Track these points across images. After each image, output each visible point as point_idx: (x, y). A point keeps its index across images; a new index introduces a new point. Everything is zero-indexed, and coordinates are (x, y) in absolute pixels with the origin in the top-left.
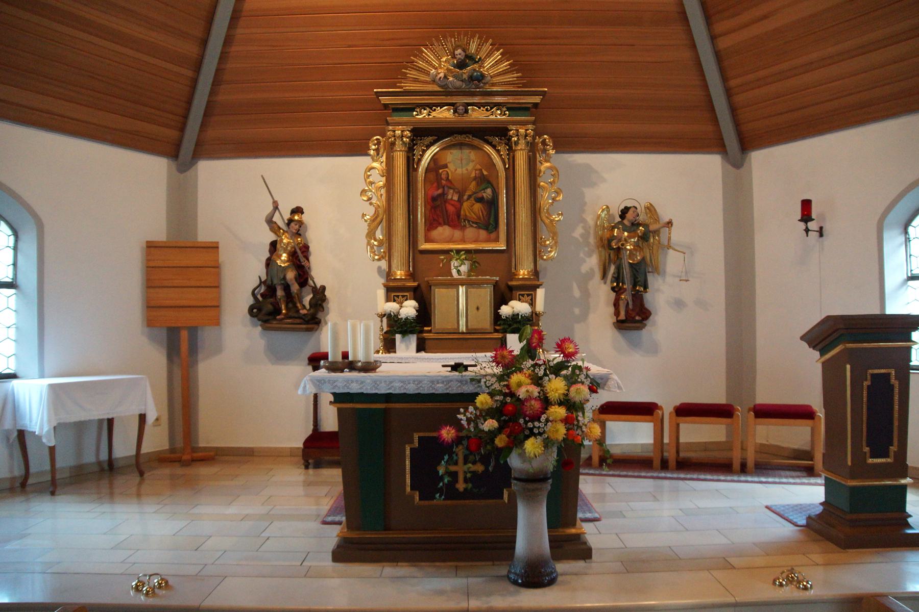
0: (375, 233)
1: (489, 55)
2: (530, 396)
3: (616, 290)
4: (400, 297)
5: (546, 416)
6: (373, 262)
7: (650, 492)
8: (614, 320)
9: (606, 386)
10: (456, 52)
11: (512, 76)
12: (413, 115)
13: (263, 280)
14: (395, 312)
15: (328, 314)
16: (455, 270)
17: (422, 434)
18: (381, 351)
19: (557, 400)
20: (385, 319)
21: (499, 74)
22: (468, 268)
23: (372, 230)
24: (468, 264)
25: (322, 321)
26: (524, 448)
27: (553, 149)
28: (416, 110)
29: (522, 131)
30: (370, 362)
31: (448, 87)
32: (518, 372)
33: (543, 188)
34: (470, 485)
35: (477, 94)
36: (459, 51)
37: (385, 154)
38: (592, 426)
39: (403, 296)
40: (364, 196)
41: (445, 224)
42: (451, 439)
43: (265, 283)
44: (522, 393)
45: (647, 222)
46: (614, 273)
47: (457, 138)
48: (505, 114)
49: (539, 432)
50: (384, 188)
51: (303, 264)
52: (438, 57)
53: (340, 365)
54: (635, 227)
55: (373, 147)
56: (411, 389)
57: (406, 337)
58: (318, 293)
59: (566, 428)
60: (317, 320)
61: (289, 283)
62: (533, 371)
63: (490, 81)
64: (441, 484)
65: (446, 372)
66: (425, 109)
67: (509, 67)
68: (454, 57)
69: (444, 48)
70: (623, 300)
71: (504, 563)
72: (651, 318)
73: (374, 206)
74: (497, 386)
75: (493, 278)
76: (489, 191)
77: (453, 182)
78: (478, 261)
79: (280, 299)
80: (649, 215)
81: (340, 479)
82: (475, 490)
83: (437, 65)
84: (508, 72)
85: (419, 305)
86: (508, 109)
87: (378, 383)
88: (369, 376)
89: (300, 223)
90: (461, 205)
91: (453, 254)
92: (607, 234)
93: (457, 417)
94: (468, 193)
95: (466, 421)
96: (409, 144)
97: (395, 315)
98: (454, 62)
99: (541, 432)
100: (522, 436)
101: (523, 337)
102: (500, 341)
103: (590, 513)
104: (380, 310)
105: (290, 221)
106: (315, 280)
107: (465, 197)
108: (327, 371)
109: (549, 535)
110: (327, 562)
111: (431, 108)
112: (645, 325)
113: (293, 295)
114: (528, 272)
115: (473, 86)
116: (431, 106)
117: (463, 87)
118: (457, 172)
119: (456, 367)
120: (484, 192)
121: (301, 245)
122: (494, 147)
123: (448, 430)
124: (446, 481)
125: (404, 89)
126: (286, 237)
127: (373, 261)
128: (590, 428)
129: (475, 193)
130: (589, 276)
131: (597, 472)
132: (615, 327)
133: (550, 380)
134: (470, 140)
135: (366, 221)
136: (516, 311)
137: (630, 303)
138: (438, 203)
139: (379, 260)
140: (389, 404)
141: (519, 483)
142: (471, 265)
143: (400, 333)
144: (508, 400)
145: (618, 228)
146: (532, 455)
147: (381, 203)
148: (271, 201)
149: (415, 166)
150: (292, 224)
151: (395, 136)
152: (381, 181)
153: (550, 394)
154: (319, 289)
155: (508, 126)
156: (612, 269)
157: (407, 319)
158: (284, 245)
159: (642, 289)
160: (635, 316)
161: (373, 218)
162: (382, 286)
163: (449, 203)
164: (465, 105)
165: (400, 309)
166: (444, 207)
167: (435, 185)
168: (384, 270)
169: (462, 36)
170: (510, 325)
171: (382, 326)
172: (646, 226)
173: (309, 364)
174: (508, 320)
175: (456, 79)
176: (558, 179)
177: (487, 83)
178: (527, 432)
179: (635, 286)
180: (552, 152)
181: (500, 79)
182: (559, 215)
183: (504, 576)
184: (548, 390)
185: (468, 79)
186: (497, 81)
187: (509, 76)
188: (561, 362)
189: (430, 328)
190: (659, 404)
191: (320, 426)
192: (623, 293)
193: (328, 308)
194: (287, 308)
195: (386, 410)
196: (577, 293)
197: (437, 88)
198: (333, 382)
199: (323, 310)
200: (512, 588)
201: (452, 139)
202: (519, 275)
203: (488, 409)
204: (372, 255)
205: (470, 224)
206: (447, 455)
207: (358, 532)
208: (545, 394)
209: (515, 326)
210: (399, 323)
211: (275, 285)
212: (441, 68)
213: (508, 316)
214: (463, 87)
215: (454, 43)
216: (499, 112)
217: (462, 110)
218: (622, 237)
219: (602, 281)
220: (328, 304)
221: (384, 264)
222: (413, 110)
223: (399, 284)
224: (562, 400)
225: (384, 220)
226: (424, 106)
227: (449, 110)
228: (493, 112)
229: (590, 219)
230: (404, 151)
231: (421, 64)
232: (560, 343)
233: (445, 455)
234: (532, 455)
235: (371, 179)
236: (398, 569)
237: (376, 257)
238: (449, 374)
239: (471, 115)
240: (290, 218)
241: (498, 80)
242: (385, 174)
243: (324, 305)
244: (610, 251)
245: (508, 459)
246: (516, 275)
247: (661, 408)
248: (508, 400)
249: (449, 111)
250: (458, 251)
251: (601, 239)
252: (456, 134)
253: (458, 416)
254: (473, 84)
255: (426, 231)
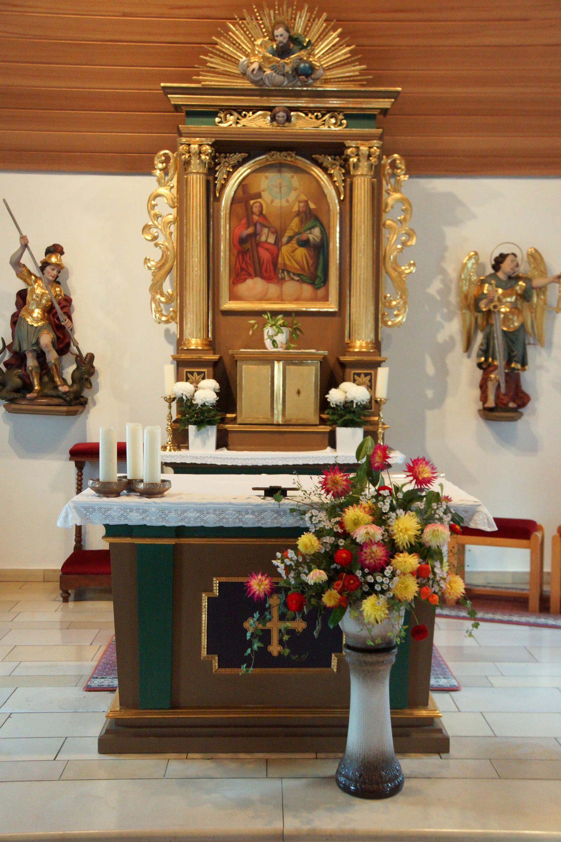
0: (162, 285)
1: (323, 36)
2: (371, 540)
3: (484, 366)
4: (195, 374)
5: (392, 568)
6: (159, 325)
7: (525, 647)
8: (480, 405)
9: (472, 521)
10: (277, 32)
11: (353, 68)
12: (215, 121)
13: (7, 344)
14: (188, 395)
15: (97, 391)
16: (269, 340)
17: (224, 579)
18: (168, 448)
19: (407, 544)
20: (174, 404)
21: (335, 65)
22: (286, 337)
23: (158, 282)
24: (287, 332)
25: (90, 401)
26: (361, 610)
27: (405, 174)
28: (219, 115)
29: (364, 149)
30: (156, 484)
31: (264, 83)
32: (355, 505)
33: (390, 228)
34: (287, 651)
35: (303, 94)
36: (280, 31)
37: (176, 176)
38: (454, 579)
39: (199, 373)
40: (147, 234)
41: (256, 276)
42: (263, 594)
43: (10, 347)
44: (360, 535)
45: (530, 275)
46: (482, 344)
47: (275, 157)
48: (341, 124)
49: (382, 589)
50: (174, 224)
51: (63, 324)
52: (250, 38)
53: (115, 487)
54: (514, 282)
55: (160, 166)
56: (211, 521)
57: (203, 430)
58: (85, 364)
59: (418, 583)
60: (82, 400)
61: (43, 349)
62: (375, 504)
63: (322, 75)
64: (249, 651)
65: (257, 499)
66: (231, 115)
67: (349, 55)
68: (273, 39)
69: (260, 25)
70: (492, 380)
71: (331, 755)
72: (530, 404)
73: (161, 248)
74: (327, 525)
75: (320, 352)
76: (317, 231)
77: (268, 217)
78: (301, 329)
79: (31, 372)
80: (533, 266)
81: (111, 618)
82: (294, 658)
83: (249, 51)
84: (349, 63)
85: (220, 386)
86: (346, 117)
87: (166, 512)
88: (155, 503)
89: (59, 267)
90: (279, 250)
91: (266, 317)
92: (474, 291)
93: (272, 563)
94: (288, 233)
95: (284, 570)
96: (209, 163)
97: (188, 400)
98: (272, 46)
99: (385, 589)
100: (358, 593)
101: (362, 453)
102: (327, 436)
103: (445, 678)
104: (168, 393)
105: (45, 265)
106: (80, 346)
107: (285, 240)
108: (97, 495)
109: (392, 718)
110: (93, 754)
111: (240, 113)
112: (521, 415)
113: (50, 365)
114: (367, 343)
115: (299, 83)
116: (239, 110)
117: (285, 83)
118: (274, 204)
119: (271, 492)
120: (311, 233)
121: (61, 297)
122: (325, 170)
123: (260, 580)
124: (255, 647)
125: (203, 85)
126: (39, 285)
127: (159, 323)
128: (450, 583)
129: (297, 234)
130: (449, 345)
131: (453, 613)
132: (481, 416)
133: (397, 518)
134: (292, 159)
135: (149, 268)
136: (350, 397)
137: (503, 385)
138: (248, 246)
139: (167, 322)
140: (181, 539)
141: (353, 653)
142: (291, 334)
143: (195, 423)
144: (341, 542)
145: (490, 284)
146: (372, 620)
147: (171, 244)
148: (19, 235)
149: (218, 195)
150: (48, 269)
151: (189, 152)
152: (171, 214)
153: (397, 536)
154: (86, 358)
155: (345, 142)
156: (480, 338)
157: (204, 405)
158: (38, 297)
159: (519, 366)
160: (508, 403)
161: (159, 265)
162: (171, 359)
163: (262, 247)
164: (286, 109)
165: (195, 391)
166: (255, 254)
167: (244, 221)
168: (174, 333)
169: (285, 7)
170: (341, 416)
171: (170, 413)
172: (527, 280)
173: (71, 459)
174: (339, 409)
175: (275, 72)
176: (411, 214)
177: (318, 79)
178: (366, 588)
179: (509, 362)
180: (404, 178)
181: (337, 74)
182: (410, 265)
183: (330, 778)
184: (395, 531)
185: (292, 74)
186: (332, 77)
187: (348, 69)
188: (412, 490)
189: (234, 415)
190: (539, 522)
191: (85, 542)
192: (492, 372)
193: (98, 384)
194: (41, 383)
195: (175, 546)
196: (430, 369)
197: (248, 85)
198: (105, 510)
199: (91, 388)
200: (343, 797)
201: (269, 157)
202: (354, 347)
203: (314, 555)
204: (157, 315)
205: (290, 276)
206: (257, 613)
207: (134, 711)
208: (390, 536)
209: (348, 417)
210: (193, 410)
211: (25, 351)
212: (255, 55)
213: (338, 404)
214: (285, 83)
215: (274, 18)
216: (333, 121)
217: (283, 117)
218: (494, 297)
219: (466, 354)
220: (97, 378)
221: (174, 327)
222: (215, 114)
223: (195, 356)
224: (414, 544)
225: (175, 268)
226: (230, 110)
227: (264, 116)
228: (324, 121)
229: (452, 271)
230: (202, 173)
231: (227, 48)
232: (412, 465)
233: (255, 612)
234: (372, 620)
235: (157, 210)
236: (189, 763)
237: (164, 319)
238: (260, 501)
239: (295, 125)
240: (45, 260)
241: (334, 75)
242: (176, 204)
243: (92, 379)
244: (477, 314)
245: (340, 623)
246: (350, 347)
247: (540, 528)
248: (341, 542)
249: (265, 118)
250: (274, 314)
251: (466, 297)
252: (273, 150)
253: (274, 562)
254: (299, 80)
255: (231, 283)
